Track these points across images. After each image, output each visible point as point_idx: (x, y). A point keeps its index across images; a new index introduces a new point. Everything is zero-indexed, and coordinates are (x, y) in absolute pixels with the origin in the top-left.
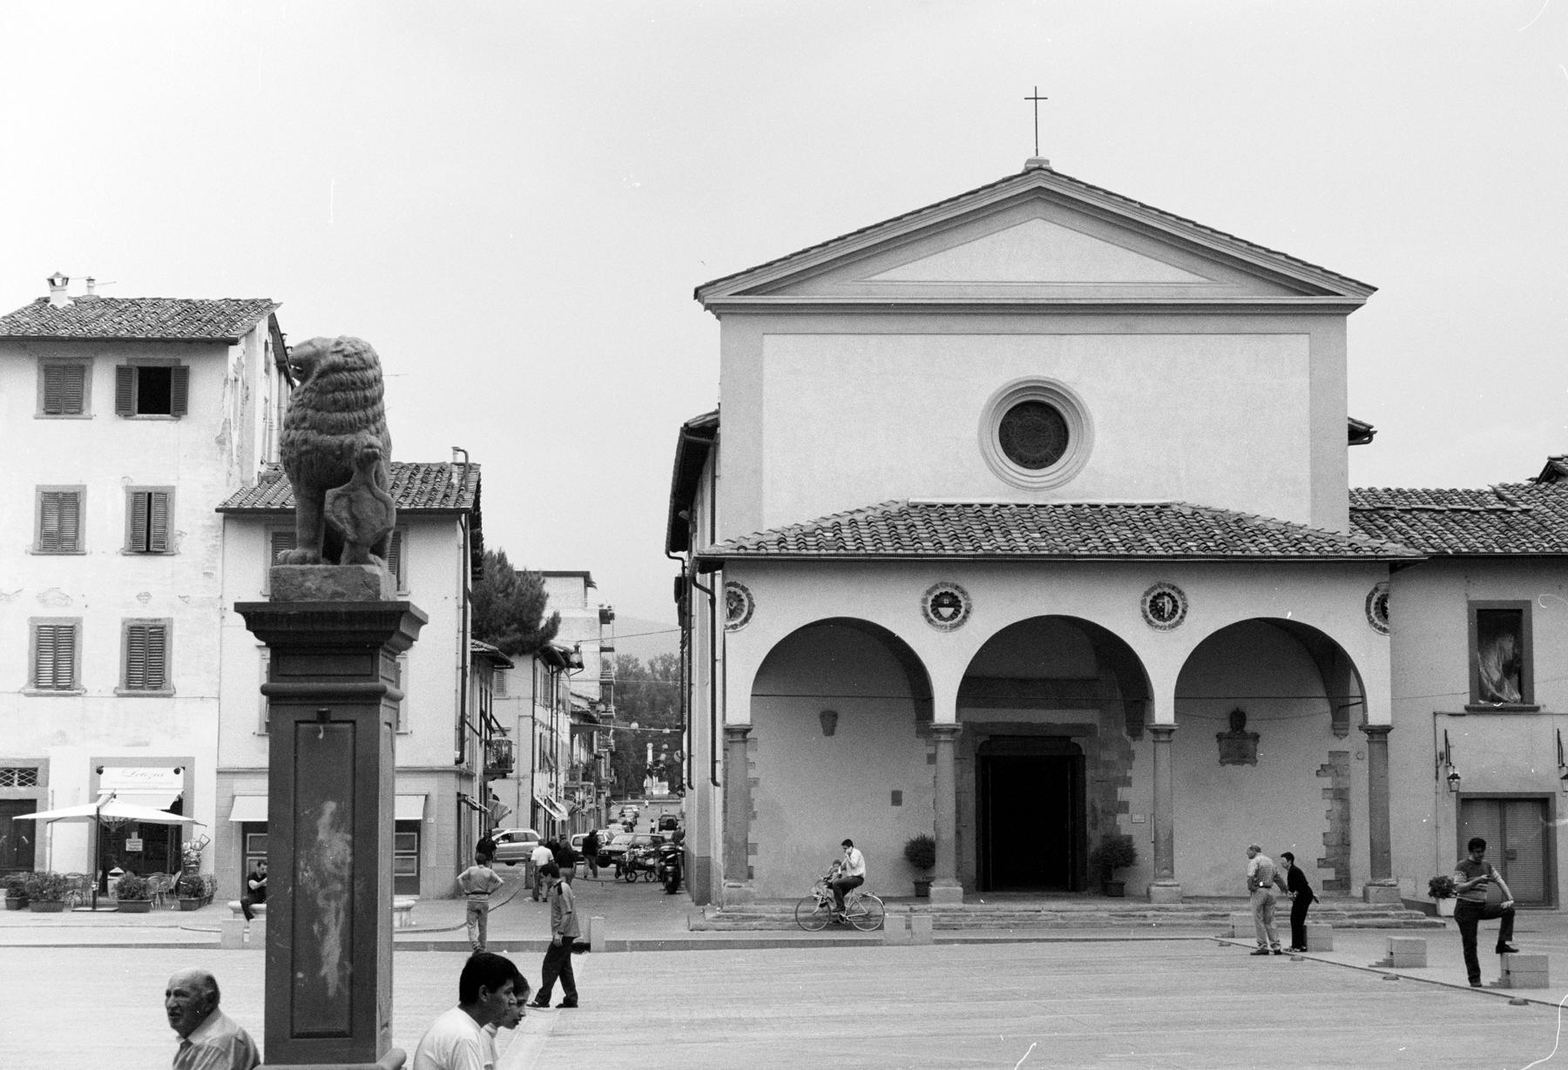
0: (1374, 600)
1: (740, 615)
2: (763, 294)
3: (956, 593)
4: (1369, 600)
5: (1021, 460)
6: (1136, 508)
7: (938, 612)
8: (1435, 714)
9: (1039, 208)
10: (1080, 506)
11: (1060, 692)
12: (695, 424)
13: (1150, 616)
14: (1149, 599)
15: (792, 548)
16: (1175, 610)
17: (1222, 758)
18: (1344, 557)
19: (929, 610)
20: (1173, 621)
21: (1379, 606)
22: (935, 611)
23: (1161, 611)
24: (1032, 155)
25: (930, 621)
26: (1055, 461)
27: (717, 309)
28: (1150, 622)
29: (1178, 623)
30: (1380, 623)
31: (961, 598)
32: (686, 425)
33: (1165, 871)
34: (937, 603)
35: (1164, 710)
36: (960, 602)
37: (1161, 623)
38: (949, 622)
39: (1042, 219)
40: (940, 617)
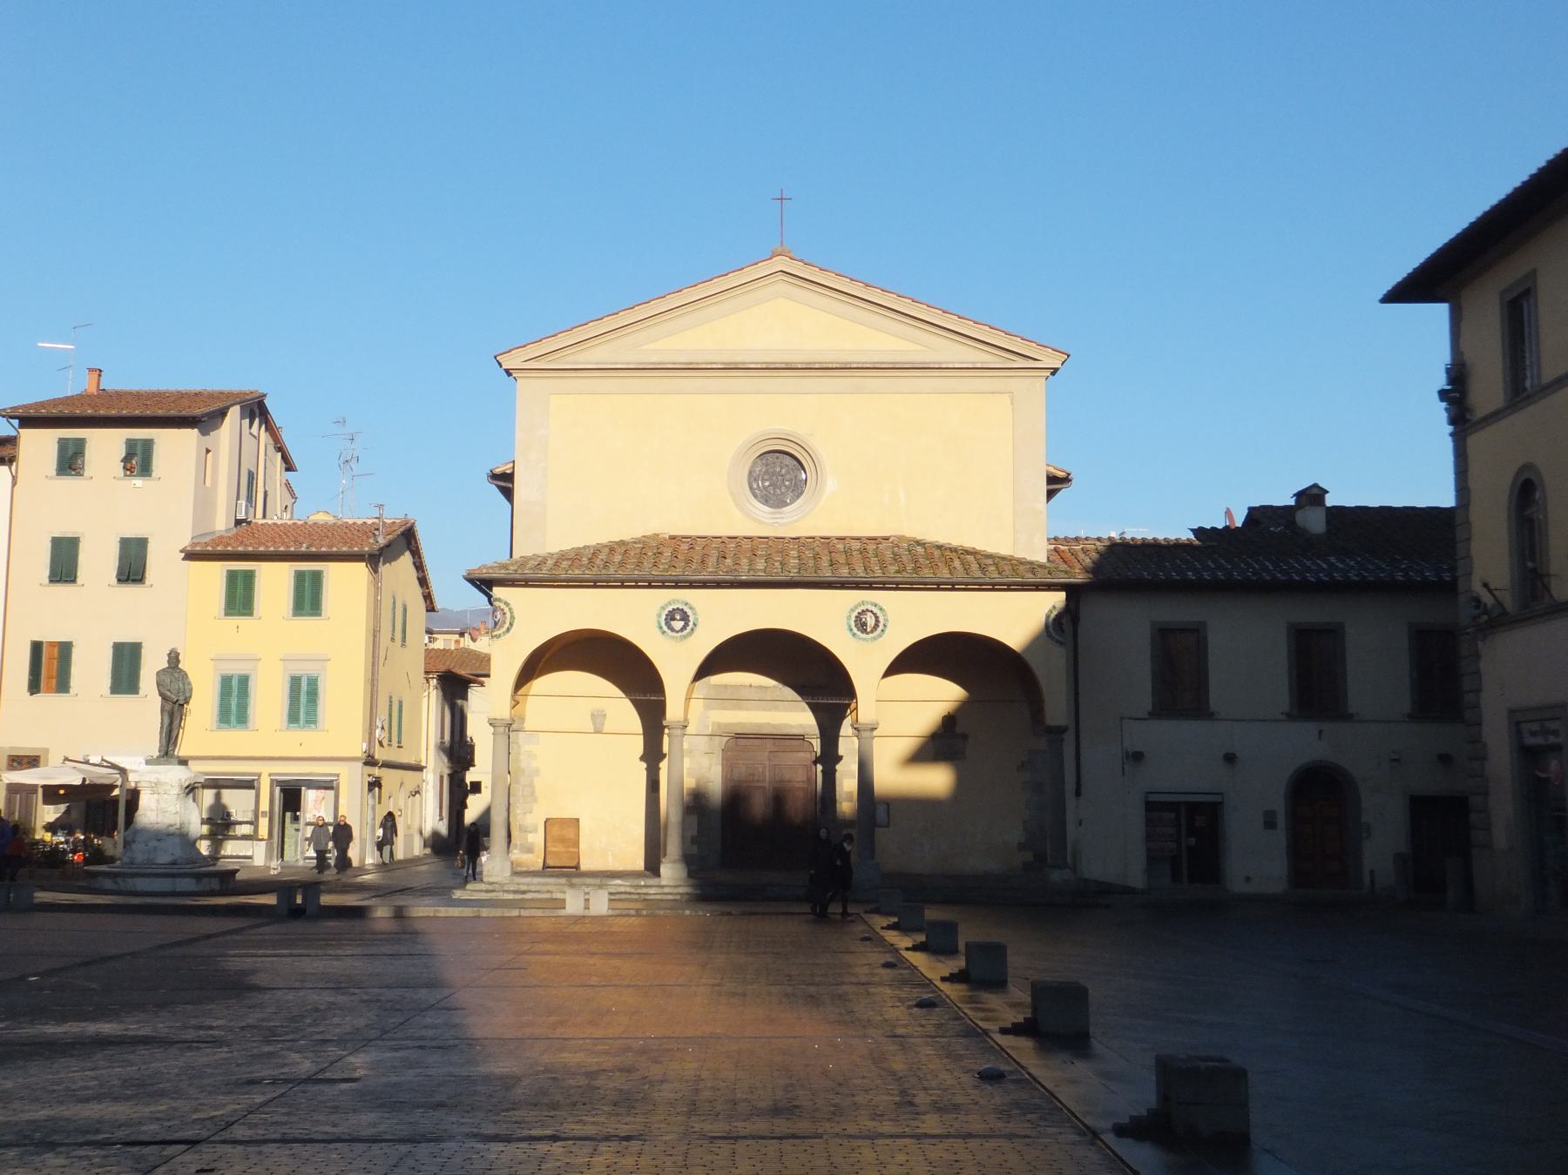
8: (1122, 719)
13: (855, 630)
14: (855, 614)
16: (876, 625)
29: (880, 636)
31: (689, 612)
34: (671, 617)
37: (864, 636)
38: (680, 634)
40: (672, 630)
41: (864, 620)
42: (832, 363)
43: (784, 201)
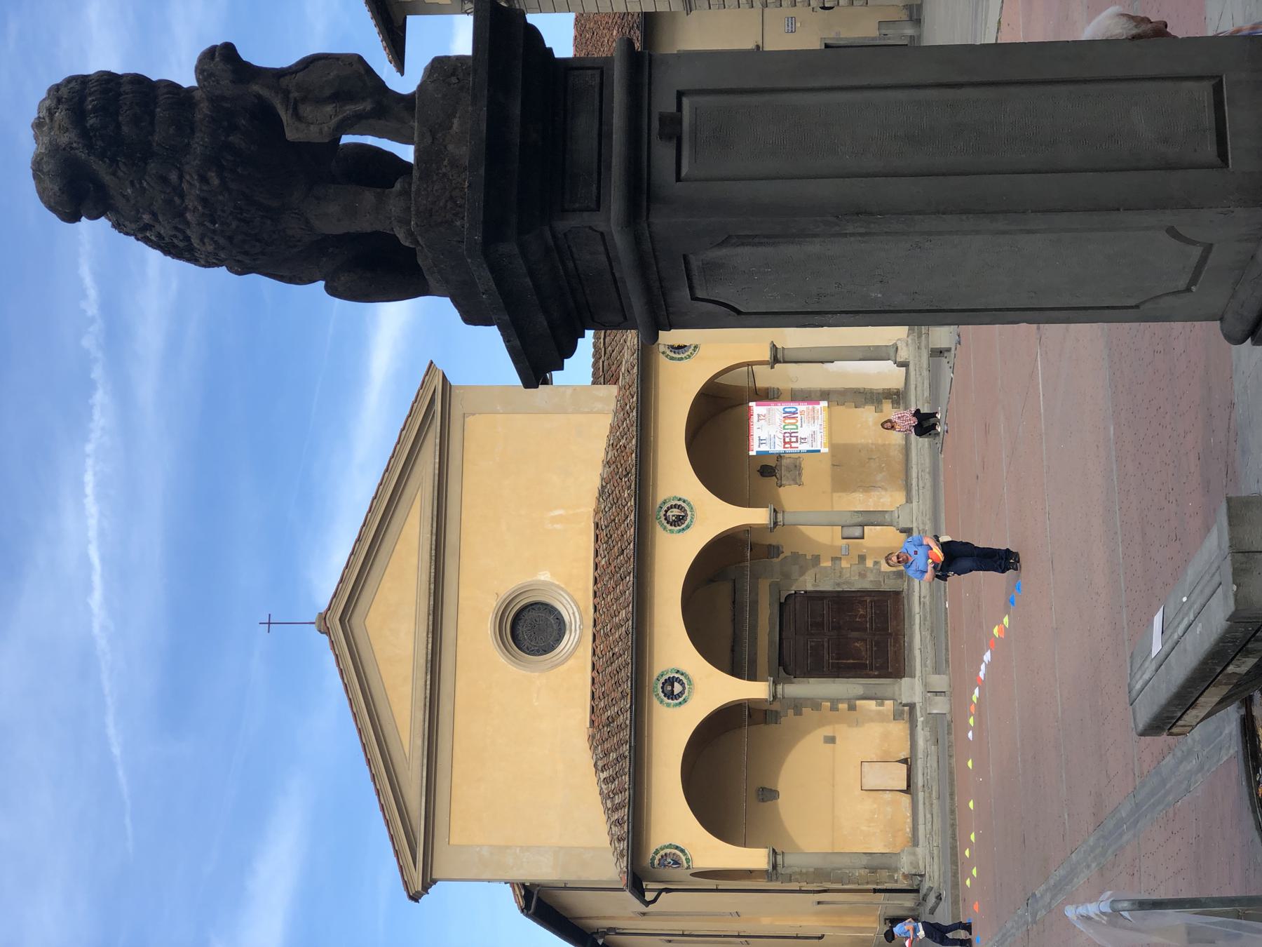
0: (672, 355)
1: (678, 856)
2: (416, 844)
3: (662, 680)
4: (672, 358)
5: (558, 640)
6: (595, 647)
7: (678, 694)
9: (356, 620)
10: (595, 593)
11: (739, 611)
12: (522, 903)
13: (683, 526)
14: (668, 526)
15: (623, 845)
16: (679, 507)
17: (796, 484)
18: (635, 537)
19: (676, 701)
20: (687, 508)
21: (676, 351)
22: (677, 697)
23: (679, 518)
24: (314, 628)
25: (685, 701)
26: (559, 613)
27: (428, 883)
28: (688, 527)
29: (689, 504)
30: (691, 350)
32: (522, 911)
33: (886, 517)
34: (671, 695)
35: (757, 516)
36: (669, 678)
37: (689, 518)
39: (365, 620)
41: (674, 518)
42: (430, 573)
43: (267, 625)
